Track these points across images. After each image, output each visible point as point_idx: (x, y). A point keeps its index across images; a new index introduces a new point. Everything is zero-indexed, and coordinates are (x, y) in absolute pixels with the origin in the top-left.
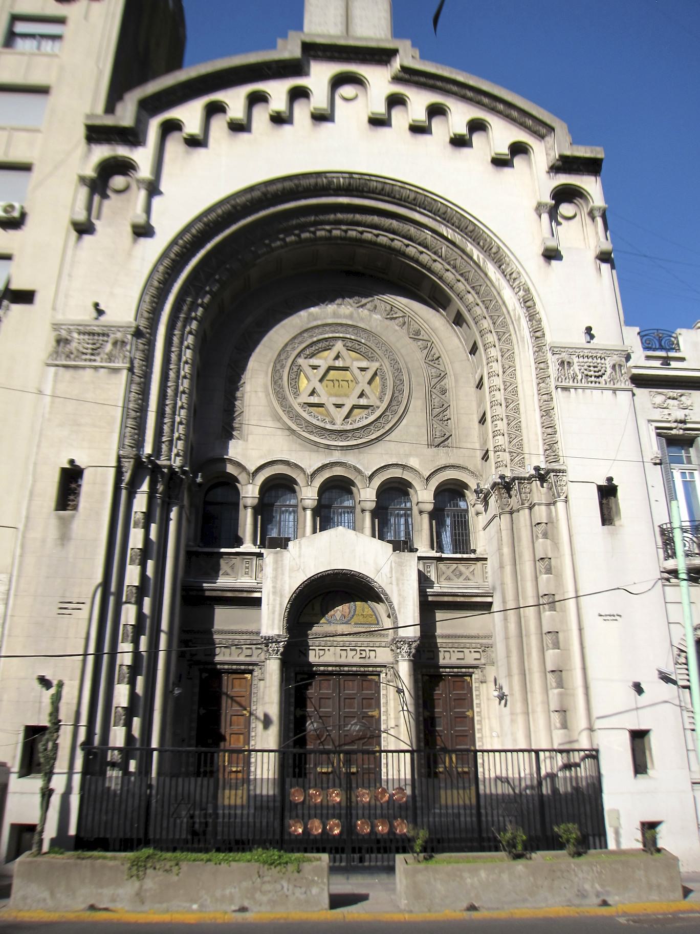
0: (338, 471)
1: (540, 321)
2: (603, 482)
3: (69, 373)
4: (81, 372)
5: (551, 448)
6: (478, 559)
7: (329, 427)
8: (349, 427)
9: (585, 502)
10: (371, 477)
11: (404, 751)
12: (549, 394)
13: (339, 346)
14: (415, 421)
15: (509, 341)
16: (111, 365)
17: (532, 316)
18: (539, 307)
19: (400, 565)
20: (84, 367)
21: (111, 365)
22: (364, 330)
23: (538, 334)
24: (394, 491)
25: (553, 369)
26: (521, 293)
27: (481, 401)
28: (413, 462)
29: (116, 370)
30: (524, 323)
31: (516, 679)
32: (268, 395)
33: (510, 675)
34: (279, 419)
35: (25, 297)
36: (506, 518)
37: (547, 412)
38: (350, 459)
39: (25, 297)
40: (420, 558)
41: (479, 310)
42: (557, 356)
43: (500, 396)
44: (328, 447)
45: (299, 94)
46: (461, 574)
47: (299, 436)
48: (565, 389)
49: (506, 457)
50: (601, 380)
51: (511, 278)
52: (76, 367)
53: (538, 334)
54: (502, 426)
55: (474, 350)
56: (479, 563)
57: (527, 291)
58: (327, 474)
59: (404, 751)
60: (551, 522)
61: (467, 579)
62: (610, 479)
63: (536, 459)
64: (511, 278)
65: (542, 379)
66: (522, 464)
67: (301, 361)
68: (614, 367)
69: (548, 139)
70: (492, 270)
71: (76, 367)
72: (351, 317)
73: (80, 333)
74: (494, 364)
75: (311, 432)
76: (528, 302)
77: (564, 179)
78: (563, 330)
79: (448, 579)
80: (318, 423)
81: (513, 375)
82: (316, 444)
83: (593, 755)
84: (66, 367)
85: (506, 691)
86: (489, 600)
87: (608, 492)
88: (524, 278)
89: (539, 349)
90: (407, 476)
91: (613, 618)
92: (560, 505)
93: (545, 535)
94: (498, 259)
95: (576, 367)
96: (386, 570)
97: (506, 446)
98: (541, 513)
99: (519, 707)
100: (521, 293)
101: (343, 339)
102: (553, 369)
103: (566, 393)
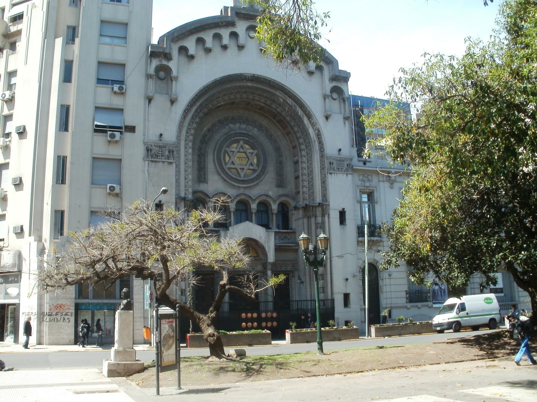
0: (243, 197)
1: (323, 144)
2: (341, 209)
3: (153, 164)
4: (158, 163)
5: (325, 196)
6: (293, 232)
7: (239, 178)
8: (246, 179)
9: (334, 216)
10: (255, 200)
11: (178, 352)
12: (325, 175)
13: (241, 143)
14: (270, 176)
15: (310, 150)
16: (169, 161)
17: (321, 143)
18: (323, 139)
19: (268, 236)
20: (159, 162)
21: (169, 161)
22: (251, 136)
23: (322, 150)
24: (264, 206)
25: (327, 165)
26: (317, 132)
27: (296, 170)
28: (270, 193)
29: (171, 163)
30: (317, 143)
31: (308, 277)
32: (215, 164)
33: (305, 275)
34: (219, 175)
35: (131, 129)
36: (306, 220)
37: (324, 182)
38: (247, 192)
39: (131, 129)
40: (275, 232)
41: (303, 147)
42: (328, 160)
43: (305, 171)
44: (239, 187)
45: (234, 35)
46: (287, 237)
47: (227, 182)
48: (331, 174)
49: (307, 196)
50: (343, 170)
51: (313, 125)
52: (156, 162)
53: (322, 150)
54: (306, 184)
55: (294, 147)
56: (293, 234)
57: (319, 131)
58: (238, 199)
59: (178, 352)
60: (323, 223)
61: (289, 239)
62: (344, 209)
63: (318, 199)
64: (313, 125)
65: (322, 168)
66: (313, 200)
67: (227, 149)
68: (347, 165)
69: (330, 65)
70: (306, 121)
71: (156, 162)
72: (245, 129)
73: (156, 146)
74: (304, 158)
75: (232, 181)
76: (319, 135)
77: (335, 84)
78: (330, 149)
79: (282, 239)
80: (231, 174)
81: (311, 164)
82: (234, 185)
83: (333, 300)
84: (152, 161)
85: (303, 279)
86: (297, 248)
87: (342, 214)
88: (318, 126)
89: (322, 156)
90: (268, 199)
91: (186, 359)
92: (326, 218)
93: (320, 228)
94: (309, 116)
95: (334, 165)
96: (263, 238)
97: (307, 192)
98: (319, 219)
99: (308, 287)
100: (317, 132)
101: (243, 140)
102: (327, 165)
103: (331, 175)
